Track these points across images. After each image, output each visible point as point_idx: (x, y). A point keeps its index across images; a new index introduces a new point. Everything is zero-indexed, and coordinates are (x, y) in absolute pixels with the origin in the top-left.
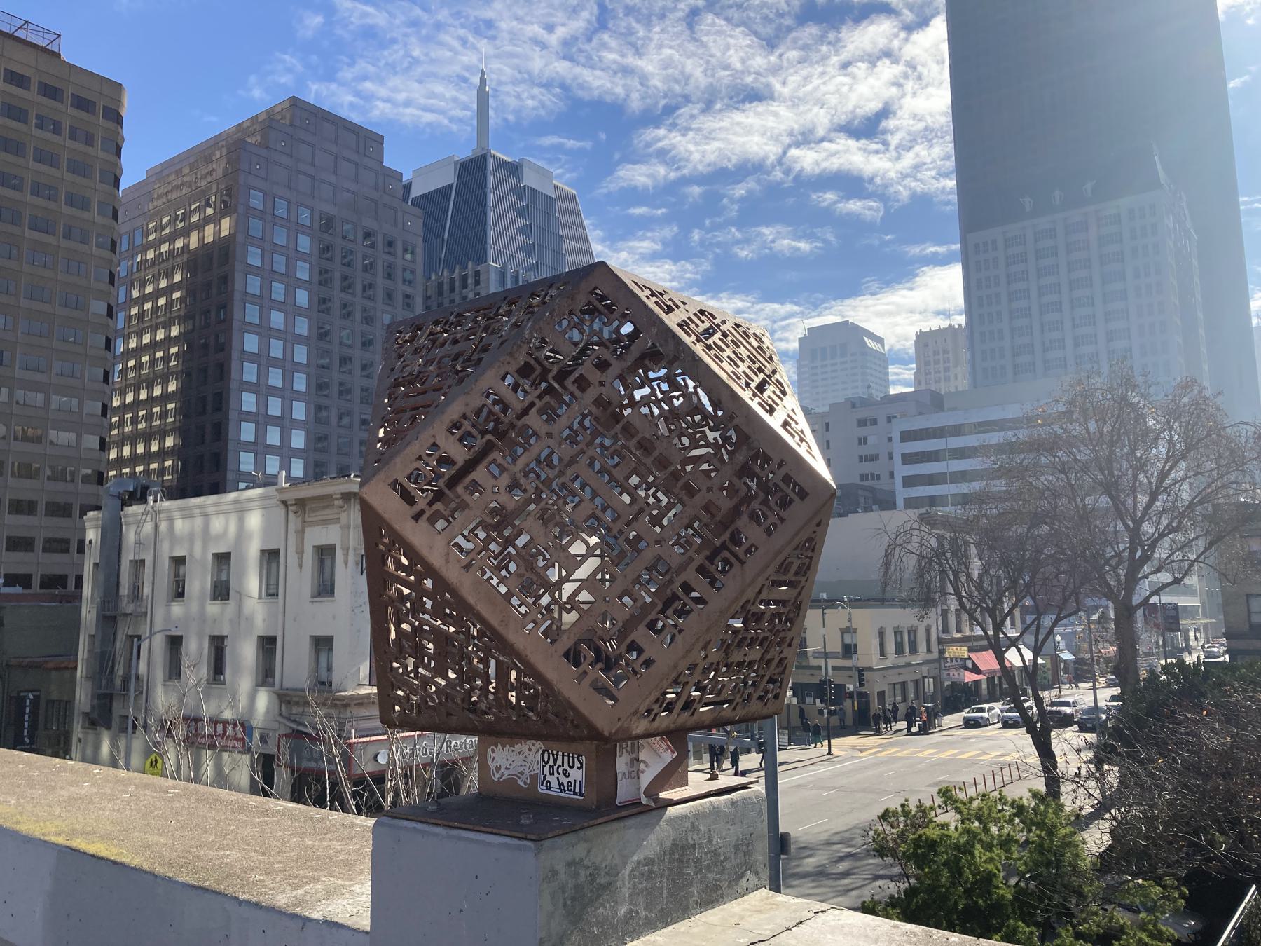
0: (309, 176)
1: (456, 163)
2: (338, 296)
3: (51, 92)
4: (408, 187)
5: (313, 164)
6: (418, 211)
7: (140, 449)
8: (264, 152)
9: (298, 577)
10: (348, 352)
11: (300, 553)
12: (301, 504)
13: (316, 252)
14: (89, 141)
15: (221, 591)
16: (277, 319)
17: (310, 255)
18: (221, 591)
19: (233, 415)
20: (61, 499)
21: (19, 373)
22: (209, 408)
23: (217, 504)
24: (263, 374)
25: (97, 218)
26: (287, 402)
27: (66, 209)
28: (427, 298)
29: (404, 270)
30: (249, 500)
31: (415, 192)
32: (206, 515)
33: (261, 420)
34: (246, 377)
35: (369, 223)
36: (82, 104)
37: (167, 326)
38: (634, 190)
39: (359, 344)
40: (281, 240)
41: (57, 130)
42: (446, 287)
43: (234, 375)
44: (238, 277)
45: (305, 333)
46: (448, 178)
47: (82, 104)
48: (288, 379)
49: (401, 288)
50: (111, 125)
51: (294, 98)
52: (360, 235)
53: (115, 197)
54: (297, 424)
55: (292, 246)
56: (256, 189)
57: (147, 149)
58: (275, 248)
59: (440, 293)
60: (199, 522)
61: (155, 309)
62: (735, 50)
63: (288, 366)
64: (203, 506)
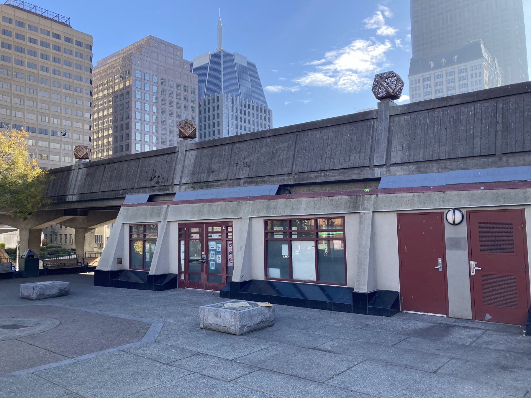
1: (210, 55)
2: (167, 108)
3: (68, 40)
4: (192, 64)
5: (158, 60)
6: (196, 76)
10: (172, 128)
14: (82, 57)
22: (124, 149)
24: (143, 137)
27: (75, 81)
28: (200, 106)
29: (191, 88)
31: (194, 66)
34: (146, 140)
35: (179, 81)
36: (79, 44)
38: (32, 367)
40: (147, 88)
41: (71, 54)
42: (207, 103)
43: (133, 138)
46: (206, 60)
47: (79, 44)
49: (190, 104)
52: (175, 85)
59: (205, 105)
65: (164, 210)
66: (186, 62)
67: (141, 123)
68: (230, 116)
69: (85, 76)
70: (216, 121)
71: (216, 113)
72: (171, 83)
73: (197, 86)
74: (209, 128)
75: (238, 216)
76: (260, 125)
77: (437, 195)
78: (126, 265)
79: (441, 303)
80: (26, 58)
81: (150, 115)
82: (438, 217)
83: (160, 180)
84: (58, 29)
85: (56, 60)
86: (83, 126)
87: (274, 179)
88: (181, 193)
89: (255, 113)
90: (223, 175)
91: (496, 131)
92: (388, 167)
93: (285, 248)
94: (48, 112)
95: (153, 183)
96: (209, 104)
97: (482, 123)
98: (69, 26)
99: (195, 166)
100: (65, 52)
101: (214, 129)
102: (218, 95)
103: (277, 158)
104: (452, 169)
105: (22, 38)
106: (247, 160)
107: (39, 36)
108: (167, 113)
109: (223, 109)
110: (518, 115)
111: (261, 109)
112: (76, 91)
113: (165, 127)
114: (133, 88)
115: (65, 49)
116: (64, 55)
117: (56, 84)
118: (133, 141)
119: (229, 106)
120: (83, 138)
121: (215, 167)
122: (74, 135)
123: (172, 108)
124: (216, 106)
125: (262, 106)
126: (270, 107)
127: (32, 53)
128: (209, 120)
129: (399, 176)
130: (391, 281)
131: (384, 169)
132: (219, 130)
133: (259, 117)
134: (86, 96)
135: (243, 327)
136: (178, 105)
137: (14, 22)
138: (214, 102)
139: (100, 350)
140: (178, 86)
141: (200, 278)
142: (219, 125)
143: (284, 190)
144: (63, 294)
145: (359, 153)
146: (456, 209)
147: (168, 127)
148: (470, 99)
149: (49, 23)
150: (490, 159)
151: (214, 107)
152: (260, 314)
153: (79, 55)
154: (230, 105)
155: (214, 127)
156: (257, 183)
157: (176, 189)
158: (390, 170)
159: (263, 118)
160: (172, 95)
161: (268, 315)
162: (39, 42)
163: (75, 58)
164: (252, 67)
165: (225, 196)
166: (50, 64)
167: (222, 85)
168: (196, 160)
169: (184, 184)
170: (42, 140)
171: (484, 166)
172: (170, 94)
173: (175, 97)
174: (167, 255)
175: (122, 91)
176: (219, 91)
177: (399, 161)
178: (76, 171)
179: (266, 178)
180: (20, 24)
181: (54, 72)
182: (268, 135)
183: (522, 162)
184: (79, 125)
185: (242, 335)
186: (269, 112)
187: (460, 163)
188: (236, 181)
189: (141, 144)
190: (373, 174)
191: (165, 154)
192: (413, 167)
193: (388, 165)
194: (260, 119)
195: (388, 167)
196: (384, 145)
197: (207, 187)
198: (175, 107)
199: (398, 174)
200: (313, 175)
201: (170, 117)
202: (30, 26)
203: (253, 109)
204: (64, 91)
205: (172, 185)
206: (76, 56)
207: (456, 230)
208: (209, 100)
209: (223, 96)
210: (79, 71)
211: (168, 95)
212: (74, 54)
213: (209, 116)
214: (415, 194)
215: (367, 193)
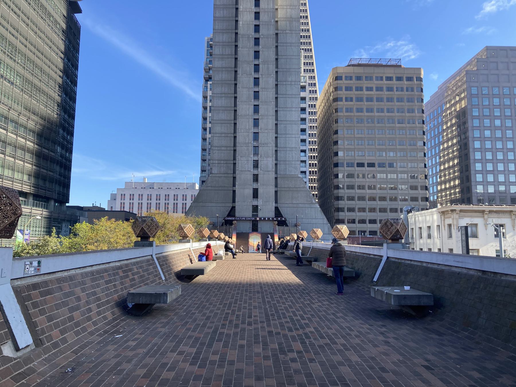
3: (399, 79)
9: (445, 232)
11: (444, 226)
15: (429, 237)
18: (429, 237)
19: (472, 172)
21: (399, 169)
23: (427, 213)
25: (417, 115)
30: (433, 212)
32: (425, 216)
36: (409, 79)
41: (402, 90)
44: (470, 121)
47: (409, 79)
50: (418, 82)
51: (487, 47)
56: (473, 87)
57: (431, 86)
60: (424, 217)
64: (424, 213)
67: (481, 141)
75: (40, 272)
80: (365, 104)
84: (390, 72)
105: (361, 89)
107: (374, 83)
112: (409, 123)
117: (391, 121)
118: (472, 161)
153: (410, 89)
162: (374, 89)
166: (385, 105)
170: (391, 173)
181: (368, 111)
204: (397, 125)
206: (407, 91)
210: (411, 104)
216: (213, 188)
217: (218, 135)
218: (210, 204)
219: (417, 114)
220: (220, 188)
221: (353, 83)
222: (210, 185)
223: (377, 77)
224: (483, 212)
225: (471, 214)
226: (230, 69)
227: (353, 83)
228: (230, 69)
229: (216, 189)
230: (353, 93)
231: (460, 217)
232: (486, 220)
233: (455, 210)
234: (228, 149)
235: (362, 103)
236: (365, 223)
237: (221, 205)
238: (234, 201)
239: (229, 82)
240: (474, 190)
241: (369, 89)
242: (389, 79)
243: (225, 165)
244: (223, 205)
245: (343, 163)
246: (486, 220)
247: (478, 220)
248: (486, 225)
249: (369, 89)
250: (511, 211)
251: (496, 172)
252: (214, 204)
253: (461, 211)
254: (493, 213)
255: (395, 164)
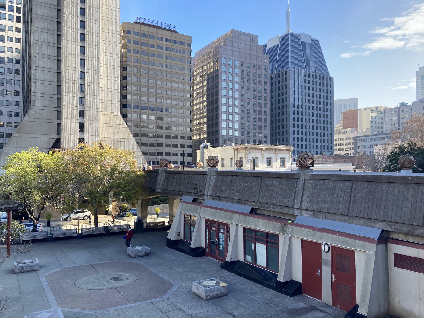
0: (237, 51)
1: (280, 37)
2: (246, 84)
3: (175, 42)
7: (198, 121)
8: (225, 47)
12: (237, 149)
13: (240, 73)
16: (230, 93)
17: (238, 74)
19: (220, 120)
20: (183, 144)
26: (234, 116)
28: (272, 79)
33: (227, 113)
35: (255, 62)
36: (182, 43)
37: (203, 97)
39: (252, 98)
40: (230, 71)
42: (277, 76)
43: (220, 118)
45: (237, 96)
46: (278, 42)
47: (182, 43)
48: (233, 78)
52: (252, 66)
53: (191, 58)
54: (236, 121)
55: (233, 72)
57: (196, 48)
58: (230, 113)
59: (275, 78)
61: (200, 92)
62: (363, 53)
63: (233, 121)
65: (199, 209)
66: (260, 46)
68: (296, 86)
69: (186, 67)
70: (284, 91)
71: (284, 84)
72: (248, 64)
73: (269, 64)
74: (279, 96)
76: (322, 91)
77: (318, 233)
78: (182, 237)
79: (318, 294)
81: (232, 91)
82: (320, 245)
83: (199, 190)
84: (168, 35)
85: (167, 58)
86: (186, 104)
87: (249, 203)
88: (208, 201)
89: (318, 82)
90: (227, 194)
91: (350, 202)
92: (301, 210)
93: (253, 245)
94: (163, 95)
95: (195, 191)
96: (279, 77)
97: (344, 195)
98: (176, 32)
99: (214, 186)
100: (173, 51)
101: (283, 97)
102: (286, 70)
103: (251, 191)
104: (328, 219)
105: (146, 45)
106: (238, 188)
107: (156, 42)
108: (246, 88)
109: (291, 81)
110: (360, 194)
111: (323, 78)
113: (243, 99)
114: (220, 72)
115: (173, 49)
116: (173, 53)
118: (220, 112)
119: (296, 77)
120: (186, 112)
121: (223, 188)
122: (180, 111)
123: (249, 85)
124: (285, 78)
125: (324, 75)
126: (331, 75)
127: (153, 55)
128: (279, 90)
129: (304, 217)
130: (298, 277)
131: (299, 211)
132: (286, 98)
133: (322, 84)
134: (187, 81)
135: (207, 296)
136: (254, 82)
137: (140, 34)
138: (283, 76)
139: (144, 300)
140: (254, 66)
141: (215, 253)
142: (286, 94)
143: (253, 212)
144: (147, 255)
145: (289, 198)
146: (325, 244)
147: (246, 99)
148: (341, 179)
149: (162, 32)
150: (346, 218)
151: (283, 80)
152: (217, 290)
154: (296, 77)
155: (283, 95)
156: (242, 204)
157: (206, 197)
158: (301, 212)
159: (325, 85)
160: (249, 74)
161: (223, 291)
162: (156, 47)
163: (180, 54)
164: (316, 43)
165: (227, 208)
167: (290, 61)
168: (215, 182)
169: (209, 196)
171: (342, 221)
172: (247, 73)
173: (251, 75)
174: (200, 238)
175: (213, 75)
176: (287, 67)
177: (305, 208)
178: (161, 174)
179: (246, 202)
180: (144, 35)
182: (249, 175)
183: (359, 223)
184: (183, 103)
185: (207, 300)
186: (330, 79)
187: (332, 216)
188: (232, 200)
189: (226, 114)
190: (294, 213)
191: (201, 175)
192: (311, 213)
193: (300, 209)
194: (322, 86)
195: (301, 210)
196: (300, 196)
197: (220, 200)
198: (252, 83)
199: (305, 215)
200: (267, 206)
201: (248, 92)
202: (150, 36)
203: (316, 78)
205: (204, 195)
207: (326, 257)
208: (279, 74)
209: (290, 70)
211: (246, 74)
212: (179, 51)
213: (279, 87)
214: (310, 230)
215: (289, 224)
216: (36, 120)
217: (40, 69)
218: (34, 136)
219: (187, 72)
220: (44, 121)
221: (140, 38)
222: (33, 117)
223: (158, 37)
224: (262, 149)
225: (255, 150)
226: (52, 6)
227: (140, 38)
228: (52, 6)
229: (40, 121)
230: (139, 47)
231: (250, 153)
232: (276, 155)
233: (247, 148)
234: (52, 83)
235: (147, 57)
236: (178, 156)
237: (45, 136)
238: (59, 132)
239: (53, 19)
240: (220, 134)
241: (153, 46)
242: (168, 40)
243: (48, 99)
244: (48, 136)
245: (131, 105)
246: (276, 155)
247: (258, 155)
248: (263, 158)
249: (153, 46)
250: (276, 149)
251: (234, 121)
252: (38, 136)
253: (250, 148)
254: (267, 150)
255: (170, 110)
